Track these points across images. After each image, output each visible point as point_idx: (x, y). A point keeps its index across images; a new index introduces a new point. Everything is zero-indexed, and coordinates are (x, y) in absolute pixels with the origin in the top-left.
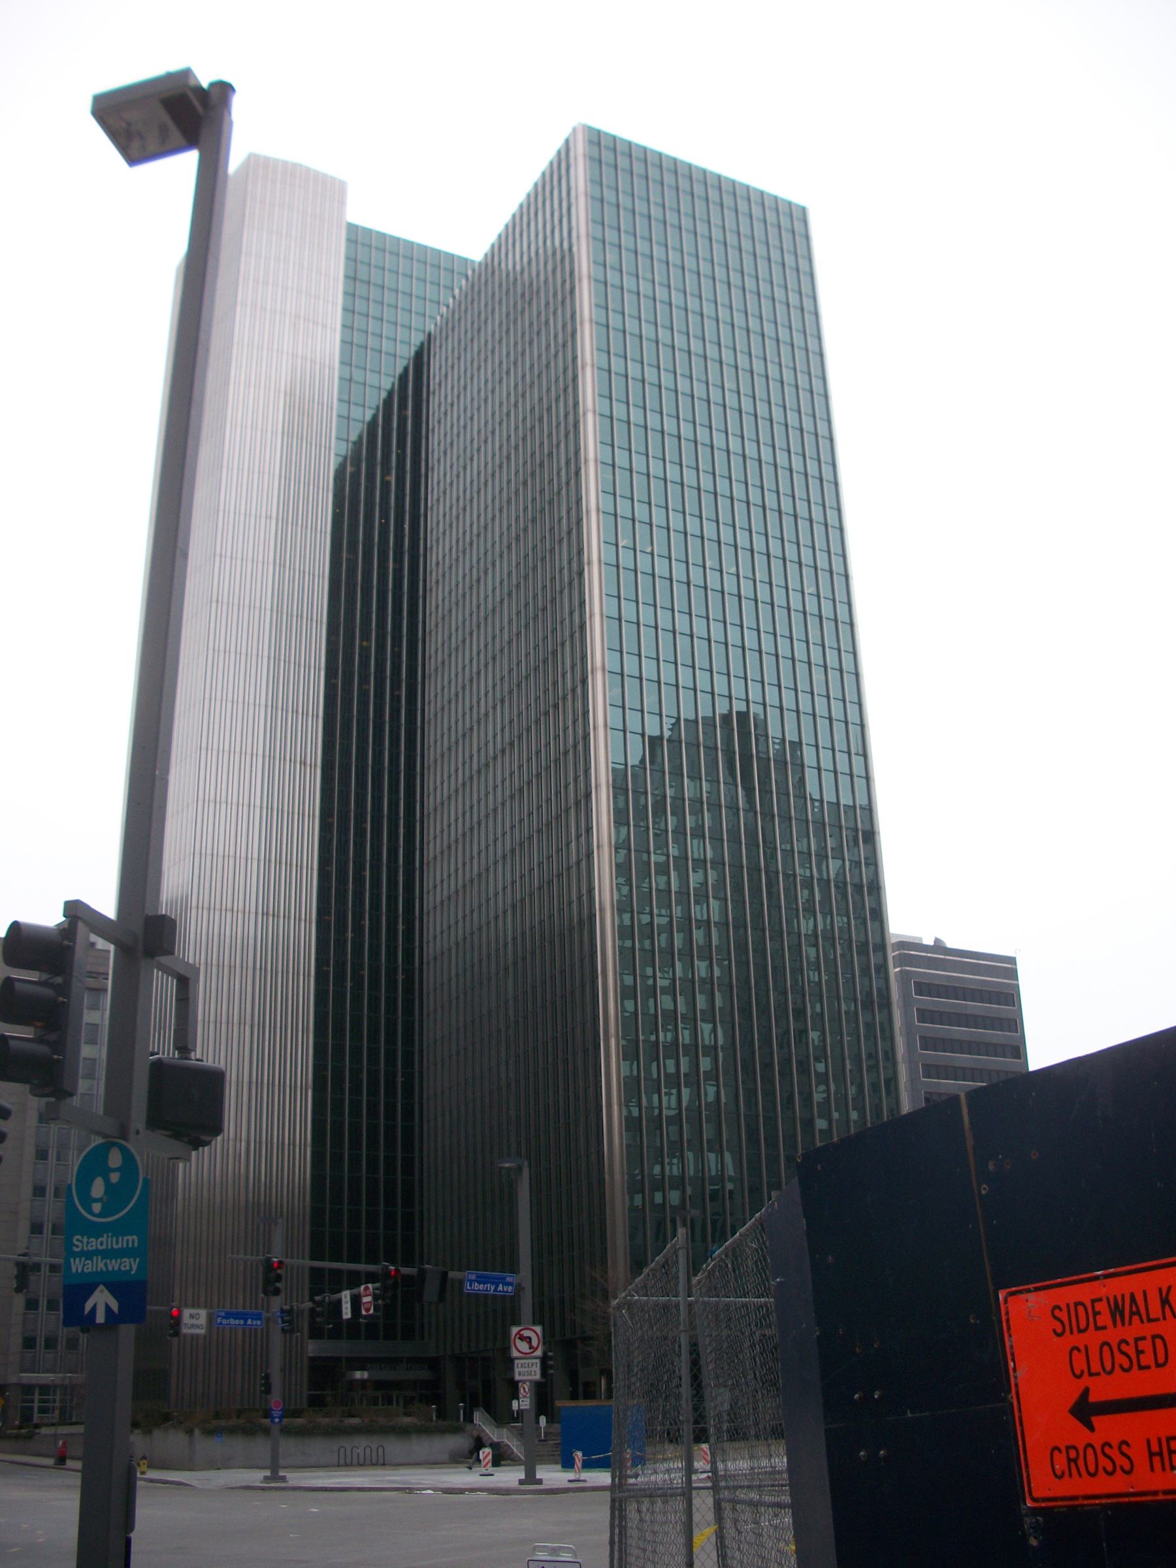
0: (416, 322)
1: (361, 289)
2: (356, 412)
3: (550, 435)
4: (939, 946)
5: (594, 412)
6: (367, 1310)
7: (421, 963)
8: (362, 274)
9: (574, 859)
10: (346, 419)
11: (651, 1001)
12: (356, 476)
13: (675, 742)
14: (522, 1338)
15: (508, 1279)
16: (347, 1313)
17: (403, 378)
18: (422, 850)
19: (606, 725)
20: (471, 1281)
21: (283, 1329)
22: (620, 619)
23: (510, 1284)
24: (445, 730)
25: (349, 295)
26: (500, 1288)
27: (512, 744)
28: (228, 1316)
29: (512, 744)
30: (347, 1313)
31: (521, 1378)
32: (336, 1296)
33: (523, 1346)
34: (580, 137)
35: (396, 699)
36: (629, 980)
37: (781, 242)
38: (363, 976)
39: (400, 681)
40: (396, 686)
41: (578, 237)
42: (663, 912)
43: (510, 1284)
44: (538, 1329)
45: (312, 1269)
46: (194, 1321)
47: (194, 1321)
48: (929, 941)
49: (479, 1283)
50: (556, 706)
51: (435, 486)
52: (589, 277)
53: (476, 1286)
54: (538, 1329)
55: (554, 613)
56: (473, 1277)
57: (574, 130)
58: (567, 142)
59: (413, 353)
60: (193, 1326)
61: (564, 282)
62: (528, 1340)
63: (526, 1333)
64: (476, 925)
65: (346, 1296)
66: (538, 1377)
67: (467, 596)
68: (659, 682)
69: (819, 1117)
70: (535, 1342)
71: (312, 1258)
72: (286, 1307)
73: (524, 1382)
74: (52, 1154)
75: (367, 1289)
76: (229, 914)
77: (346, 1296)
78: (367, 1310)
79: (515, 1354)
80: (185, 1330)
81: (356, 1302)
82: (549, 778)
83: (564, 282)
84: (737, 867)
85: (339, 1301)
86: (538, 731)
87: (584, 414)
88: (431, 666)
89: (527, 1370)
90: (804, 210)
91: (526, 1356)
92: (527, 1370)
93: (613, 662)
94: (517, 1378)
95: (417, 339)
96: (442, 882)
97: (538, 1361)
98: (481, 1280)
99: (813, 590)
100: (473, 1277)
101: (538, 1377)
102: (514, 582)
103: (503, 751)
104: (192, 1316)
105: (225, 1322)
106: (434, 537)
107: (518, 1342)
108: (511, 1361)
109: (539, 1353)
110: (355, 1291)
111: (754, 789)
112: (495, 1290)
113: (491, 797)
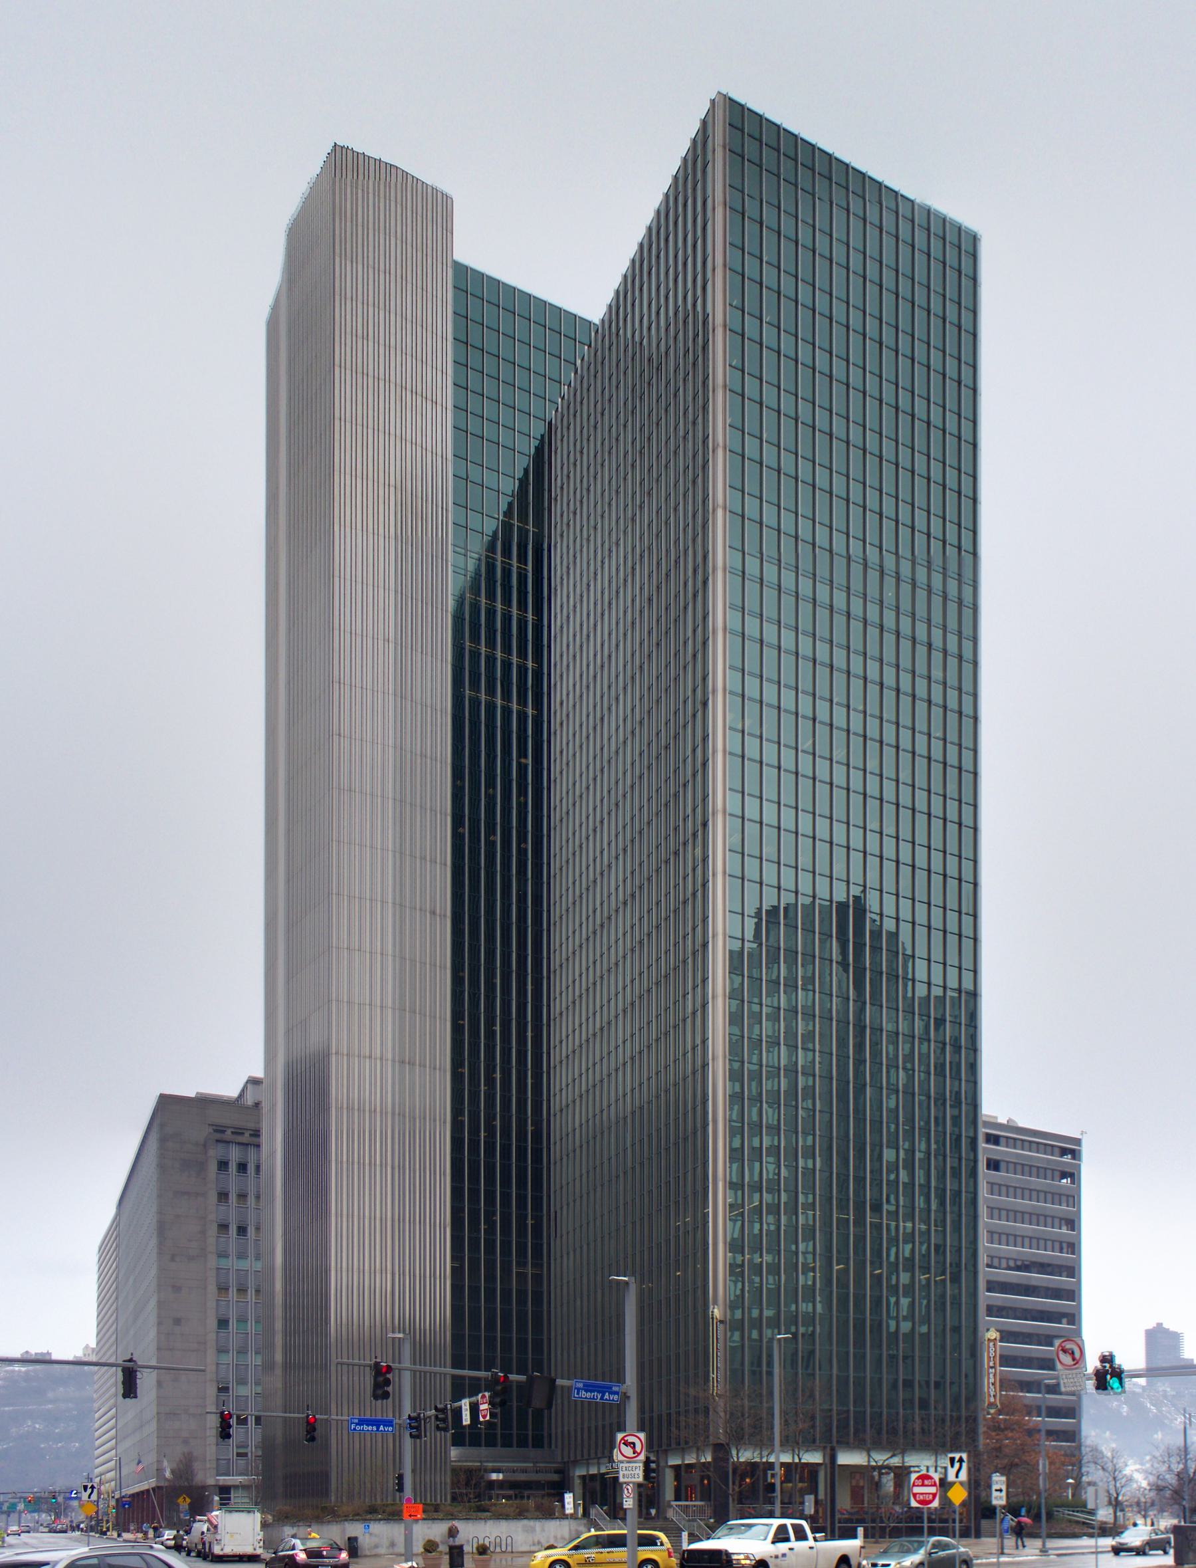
0: (535, 407)
1: (474, 358)
2: (474, 520)
3: (677, 540)
5: (725, 508)
6: (484, 1417)
8: (474, 339)
9: (690, 1010)
10: (462, 527)
11: (757, 1165)
12: (475, 607)
14: (627, 1443)
15: (615, 1389)
16: (466, 1420)
17: (523, 482)
19: (724, 872)
20: (578, 1389)
21: (411, 1434)
22: (743, 757)
23: (617, 1393)
24: (570, 885)
25: (461, 364)
26: (607, 1396)
27: (633, 896)
28: (362, 1422)
29: (633, 896)
30: (466, 1420)
31: (626, 1480)
33: (628, 1451)
34: (719, 114)
35: (522, 852)
36: (737, 1143)
37: (944, 289)
38: (495, 1126)
39: (526, 834)
40: (522, 838)
41: (714, 691)
43: (617, 1393)
44: (642, 1435)
45: (454, 1377)
48: (1002, 1120)
49: (586, 1391)
50: (676, 853)
51: (558, 610)
52: (725, 326)
53: (583, 1394)
54: (642, 1435)
55: (677, 691)
56: (581, 1385)
57: (713, 102)
58: (704, 123)
59: (533, 451)
61: (696, 336)
63: (630, 1439)
64: (598, 1078)
65: (465, 1404)
66: (641, 1479)
67: (598, 779)
68: (779, 828)
69: (803, 1301)
70: (638, 1449)
71: (454, 1366)
72: (413, 1415)
73: (627, 1483)
75: (484, 1396)
77: (465, 1404)
78: (484, 1417)
81: (474, 1409)
82: (667, 928)
83: (696, 336)
84: (843, 1022)
85: (461, 1407)
86: (667, 928)
87: (714, 510)
88: (556, 817)
90: (975, 239)
91: (630, 1460)
93: (734, 805)
94: (621, 1480)
95: (537, 429)
96: (567, 1037)
98: (588, 1388)
99: (940, 734)
100: (581, 1385)
102: (638, 718)
103: (625, 903)
105: (358, 1428)
106: (558, 672)
109: (642, 1457)
110: (474, 1399)
111: (865, 945)
112: (602, 1398)
113: (613, 950)
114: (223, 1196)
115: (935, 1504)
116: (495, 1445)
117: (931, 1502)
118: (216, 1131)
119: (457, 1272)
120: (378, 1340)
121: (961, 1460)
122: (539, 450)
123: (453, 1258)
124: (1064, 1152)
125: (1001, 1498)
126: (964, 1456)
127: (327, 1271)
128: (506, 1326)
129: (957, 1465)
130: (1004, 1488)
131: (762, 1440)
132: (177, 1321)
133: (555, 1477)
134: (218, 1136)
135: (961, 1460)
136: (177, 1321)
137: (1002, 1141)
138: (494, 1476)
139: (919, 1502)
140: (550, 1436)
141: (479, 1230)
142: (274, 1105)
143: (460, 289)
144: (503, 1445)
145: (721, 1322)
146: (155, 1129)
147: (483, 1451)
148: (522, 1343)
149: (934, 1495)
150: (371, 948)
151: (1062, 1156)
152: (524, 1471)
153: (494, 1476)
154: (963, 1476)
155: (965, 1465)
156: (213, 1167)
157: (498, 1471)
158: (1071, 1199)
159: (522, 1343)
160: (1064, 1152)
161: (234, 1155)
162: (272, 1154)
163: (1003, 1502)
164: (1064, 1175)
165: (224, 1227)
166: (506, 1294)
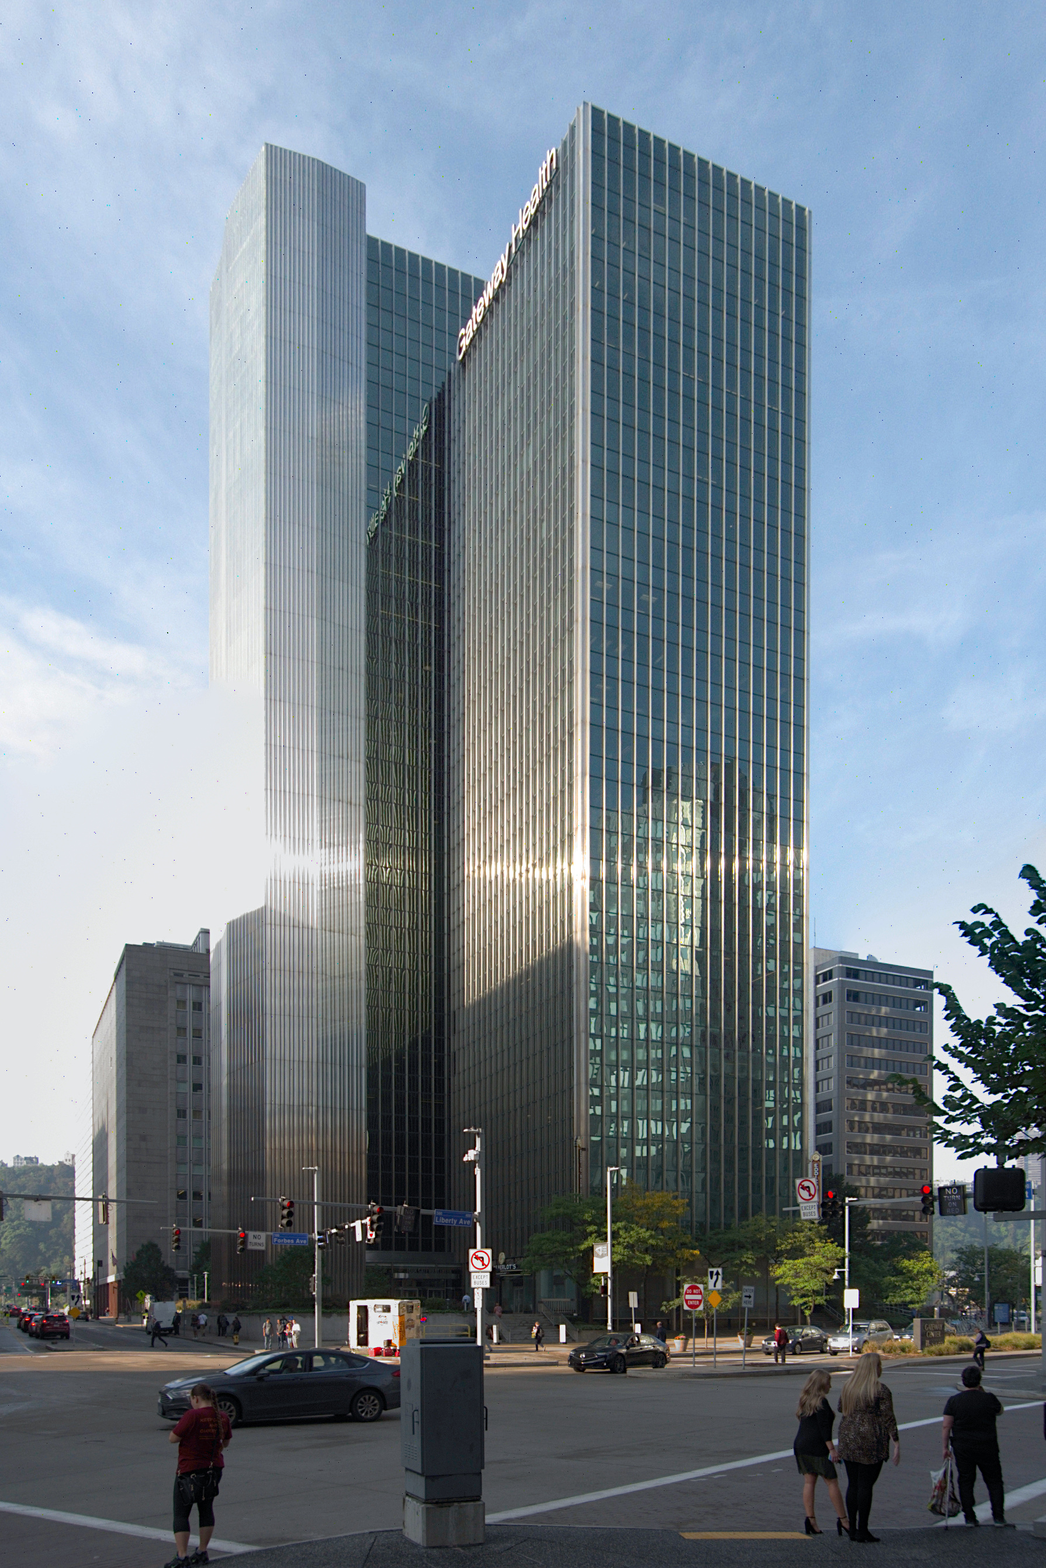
4: (871, 962)
7: (449, 971)
13: (672, 795)
15: (467, 1216)
18: (449, 878)
20: (439, 1217)
26: (461, 1221)
32: (352, 1225)
33: (478, 1263)
42: (626, 933)
44: (489, 1251)
46: (257, 1241)
47: (257, 1241)
48: (863, 957)
54: (489, 1251)
56: (440, 1214)
60: (256, 1244)
62: (807, 1188)
63: (480, 1254)
66: (488, 1285)
70: (486, 1261)
74: (189, 1113)
76: (296, 929)
79: (472, 1268)
80: (250, 1247)
89: (480, 1280)
92: (480, 1280)
97: (488, 1274)
98: (445, 1216)
101: (488, 1285)
104: (255, 1237)
105: (279, 1241)
107: (801, 1190)
108: (470, 1273)
109: (489, 1268)
114: (181, 1030)
115: (701, 1308)
116: (403, 1249)
117: (698, 1306)
118: (176, 975)
119: (371, 1103)
120: (287, 1179)
121: (717, 1274)
122: (441, 397)
123: (368, 1092)
124: (918, 983)
125: (750, 1302)
126: (720, 1270)
127: (264, 1104)
128: (413, 1151)
129: (715, 1277)
130: (752, 1295)
131: (788, 1206)
132: (143, 1138)
133: (453, 1276)
134: (178, 979)
135: (717, 1274)
136: (143, 1138)
137: (861, 975)
138: (402, 1276)
139: (689, 1306)
140: (450, 1240)
141: (409, 1055)
142: (219, 964)
143: (371, 260)
144: (410, 1249)
145: (583, 1149)
146: (124, 967)
147: (393, 1254)
148: (427, 1163)
149: (700, 1301)
150: (106, 1209)
151: (915, 987)
152: (427, 1271)
153: (402, 1276)
154: (719, 1285)
155: (720, 1277)
156: (172, 1005)
157: (404, 1271)
158: (924, 1025)
159: (427, 1163)
160: (918, 983)
161: (190, 994)
162: (219, 1005)
163: (752, 1306)
164: (918, 1004)
165: (181, 1059)
166: (413, 1123)
